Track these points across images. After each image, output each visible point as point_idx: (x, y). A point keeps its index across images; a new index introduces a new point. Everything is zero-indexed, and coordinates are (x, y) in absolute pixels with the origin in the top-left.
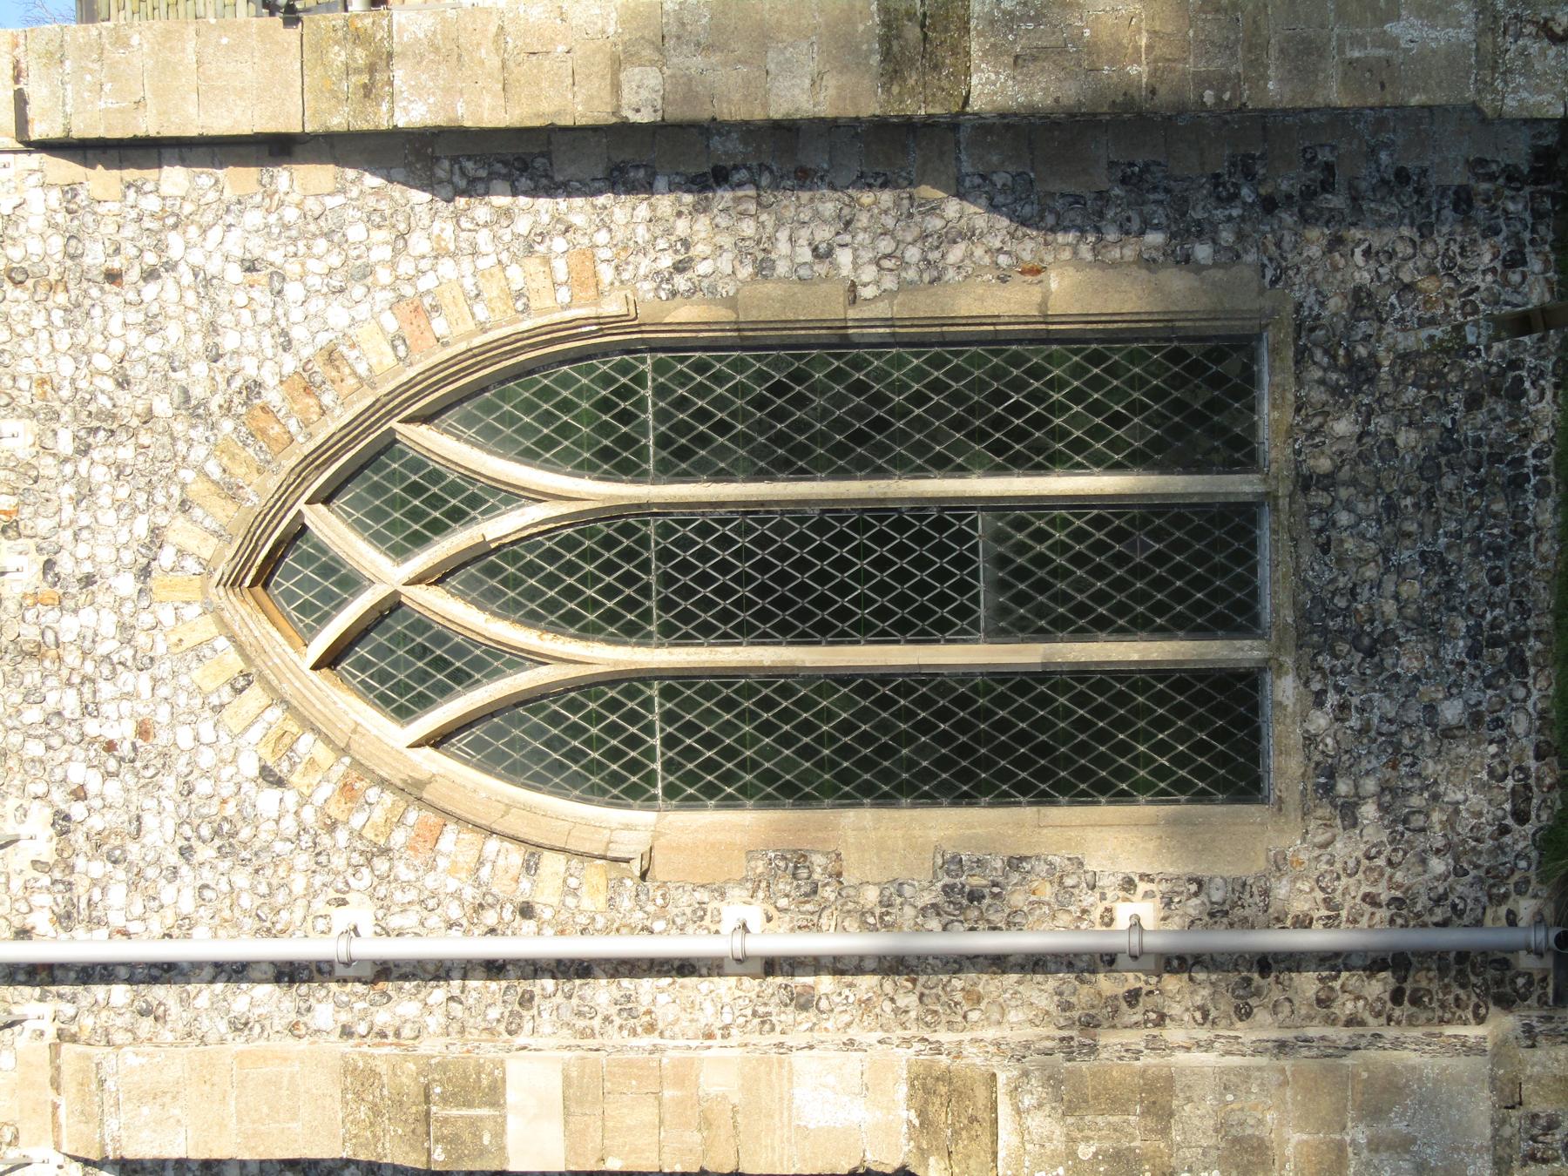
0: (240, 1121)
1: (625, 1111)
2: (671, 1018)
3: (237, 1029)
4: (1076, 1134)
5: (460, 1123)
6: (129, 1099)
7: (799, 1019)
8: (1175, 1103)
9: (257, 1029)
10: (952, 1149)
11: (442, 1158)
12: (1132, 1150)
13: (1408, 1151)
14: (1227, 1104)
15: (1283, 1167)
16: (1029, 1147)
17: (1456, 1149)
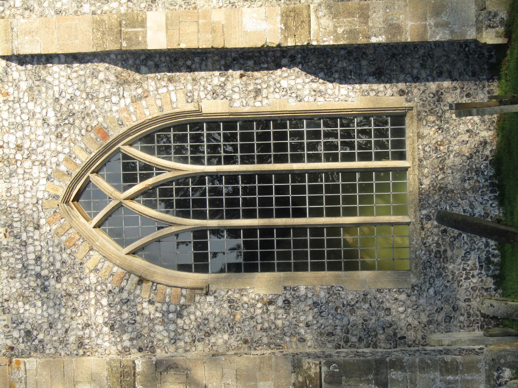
0: (58, 40)
1: (187, 28)
2: (202, 5)
3: (57, 14)
4: (337, 25)
5: (131, 34)
6: (21, 34)
7: (244, 4)
8: (370, 13)
9: (64, 13)
10: (296, 34)
11: (125, 45)
12: (355, 29)
13: (448, 27)
14: (387, 13)
15: (406, 34)
16: (321, 29)
17: (464, 26)
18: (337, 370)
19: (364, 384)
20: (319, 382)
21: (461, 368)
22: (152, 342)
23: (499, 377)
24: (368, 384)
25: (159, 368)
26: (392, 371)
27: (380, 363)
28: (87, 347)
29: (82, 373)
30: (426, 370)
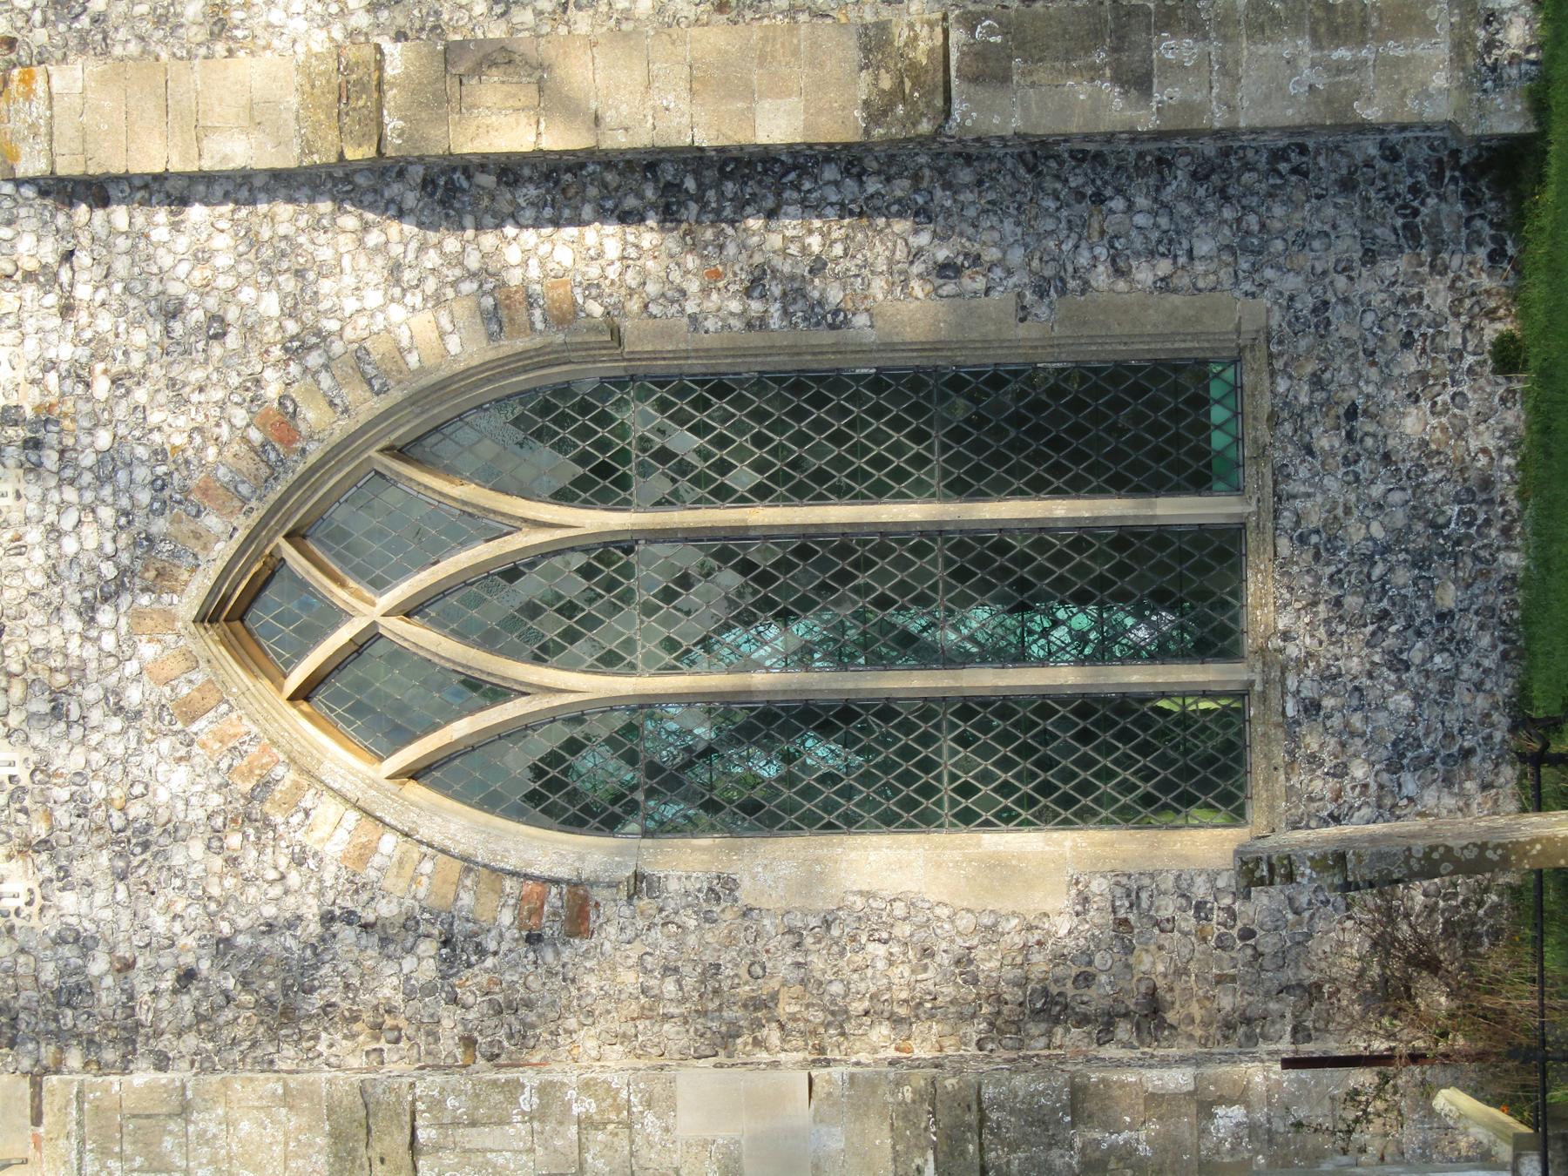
18: (999, 39)
19: (1079, 79)
20: (940, 74)
21: (1375, 23)
22: (437, 14)
23: (1490, 45)
24: (1092, 80)
25: (454, 65)
26: (1166, 39)
27: (1128, 14)
28: (239, 33)
29: (221, 100)
30: (1268, 32)
